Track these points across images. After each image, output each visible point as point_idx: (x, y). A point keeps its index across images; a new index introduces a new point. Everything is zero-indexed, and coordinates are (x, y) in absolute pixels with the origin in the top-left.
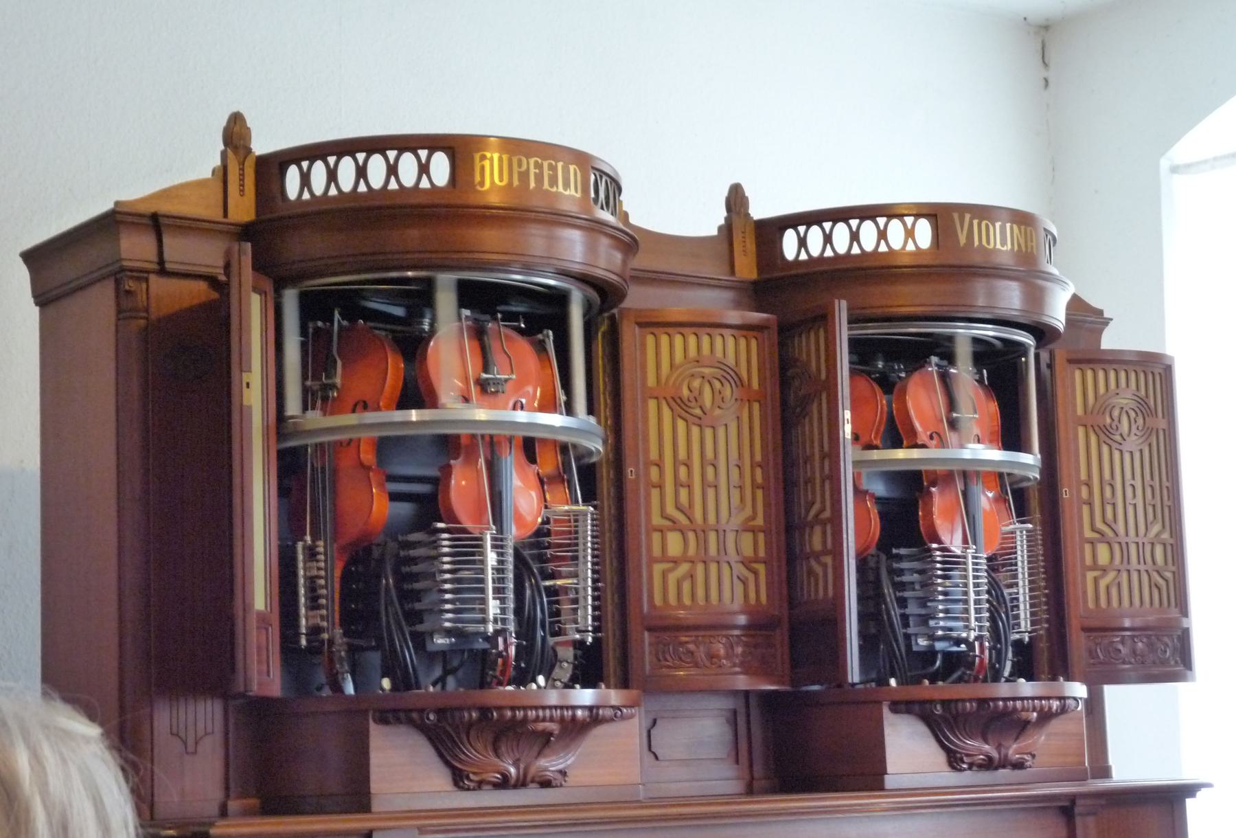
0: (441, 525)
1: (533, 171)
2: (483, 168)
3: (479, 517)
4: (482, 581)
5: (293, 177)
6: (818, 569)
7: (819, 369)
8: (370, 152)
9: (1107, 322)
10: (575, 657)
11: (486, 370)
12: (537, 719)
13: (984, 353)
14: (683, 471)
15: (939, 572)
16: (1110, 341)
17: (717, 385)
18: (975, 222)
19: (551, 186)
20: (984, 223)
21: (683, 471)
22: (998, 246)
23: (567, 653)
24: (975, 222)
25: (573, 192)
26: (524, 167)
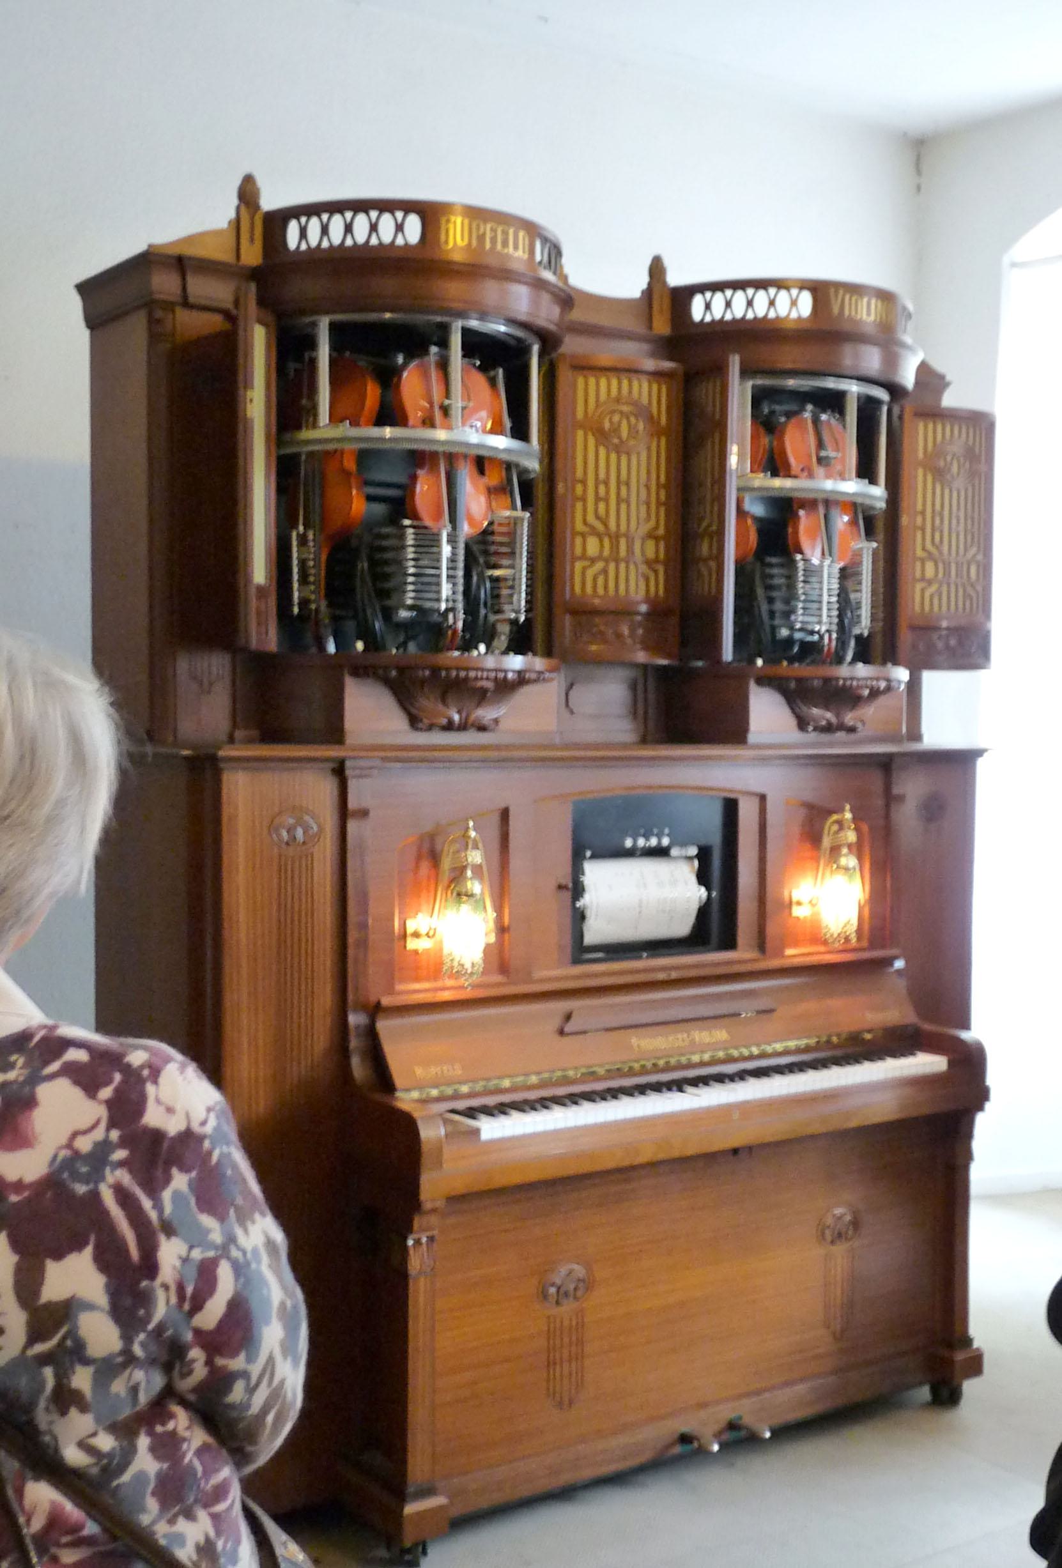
12: (476, 678)
16: (949, 400)
17: (633, 420)
18: (847, 297)
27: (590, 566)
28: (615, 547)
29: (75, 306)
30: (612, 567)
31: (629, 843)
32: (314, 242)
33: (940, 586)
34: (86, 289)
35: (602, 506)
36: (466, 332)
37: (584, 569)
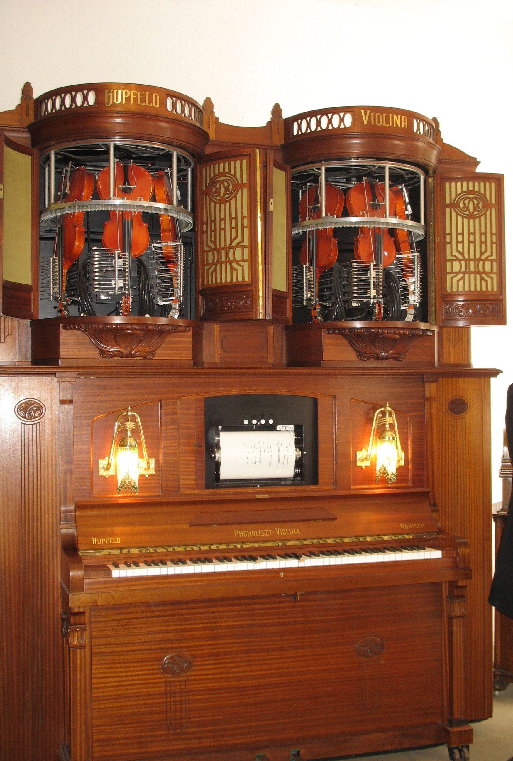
0: (353, 260)
1: (132, 96)
2: (109, 96)
3: (370, 257)
4: (369, 282)
5: (296, 126)
8: (333, 114)
9: (478, 163)
10: (414, 313)
11: (374, 200)
13: (397, 178)
14: (483, 239)
15: (355, 280)
16: (479, 169)
17: (476, 202)
18: (372, 114)
19: (142, 102)
21: (483, 239)
23: (411, 311)
24: (372, 114)
25: (154, 105)
27: (455, 276)
28: (468, 266)
30: (467, 276)
31: (246, 422)
32: (313, 129)
33: (217, 266)
35: (460, 246)
36: (116, 147)
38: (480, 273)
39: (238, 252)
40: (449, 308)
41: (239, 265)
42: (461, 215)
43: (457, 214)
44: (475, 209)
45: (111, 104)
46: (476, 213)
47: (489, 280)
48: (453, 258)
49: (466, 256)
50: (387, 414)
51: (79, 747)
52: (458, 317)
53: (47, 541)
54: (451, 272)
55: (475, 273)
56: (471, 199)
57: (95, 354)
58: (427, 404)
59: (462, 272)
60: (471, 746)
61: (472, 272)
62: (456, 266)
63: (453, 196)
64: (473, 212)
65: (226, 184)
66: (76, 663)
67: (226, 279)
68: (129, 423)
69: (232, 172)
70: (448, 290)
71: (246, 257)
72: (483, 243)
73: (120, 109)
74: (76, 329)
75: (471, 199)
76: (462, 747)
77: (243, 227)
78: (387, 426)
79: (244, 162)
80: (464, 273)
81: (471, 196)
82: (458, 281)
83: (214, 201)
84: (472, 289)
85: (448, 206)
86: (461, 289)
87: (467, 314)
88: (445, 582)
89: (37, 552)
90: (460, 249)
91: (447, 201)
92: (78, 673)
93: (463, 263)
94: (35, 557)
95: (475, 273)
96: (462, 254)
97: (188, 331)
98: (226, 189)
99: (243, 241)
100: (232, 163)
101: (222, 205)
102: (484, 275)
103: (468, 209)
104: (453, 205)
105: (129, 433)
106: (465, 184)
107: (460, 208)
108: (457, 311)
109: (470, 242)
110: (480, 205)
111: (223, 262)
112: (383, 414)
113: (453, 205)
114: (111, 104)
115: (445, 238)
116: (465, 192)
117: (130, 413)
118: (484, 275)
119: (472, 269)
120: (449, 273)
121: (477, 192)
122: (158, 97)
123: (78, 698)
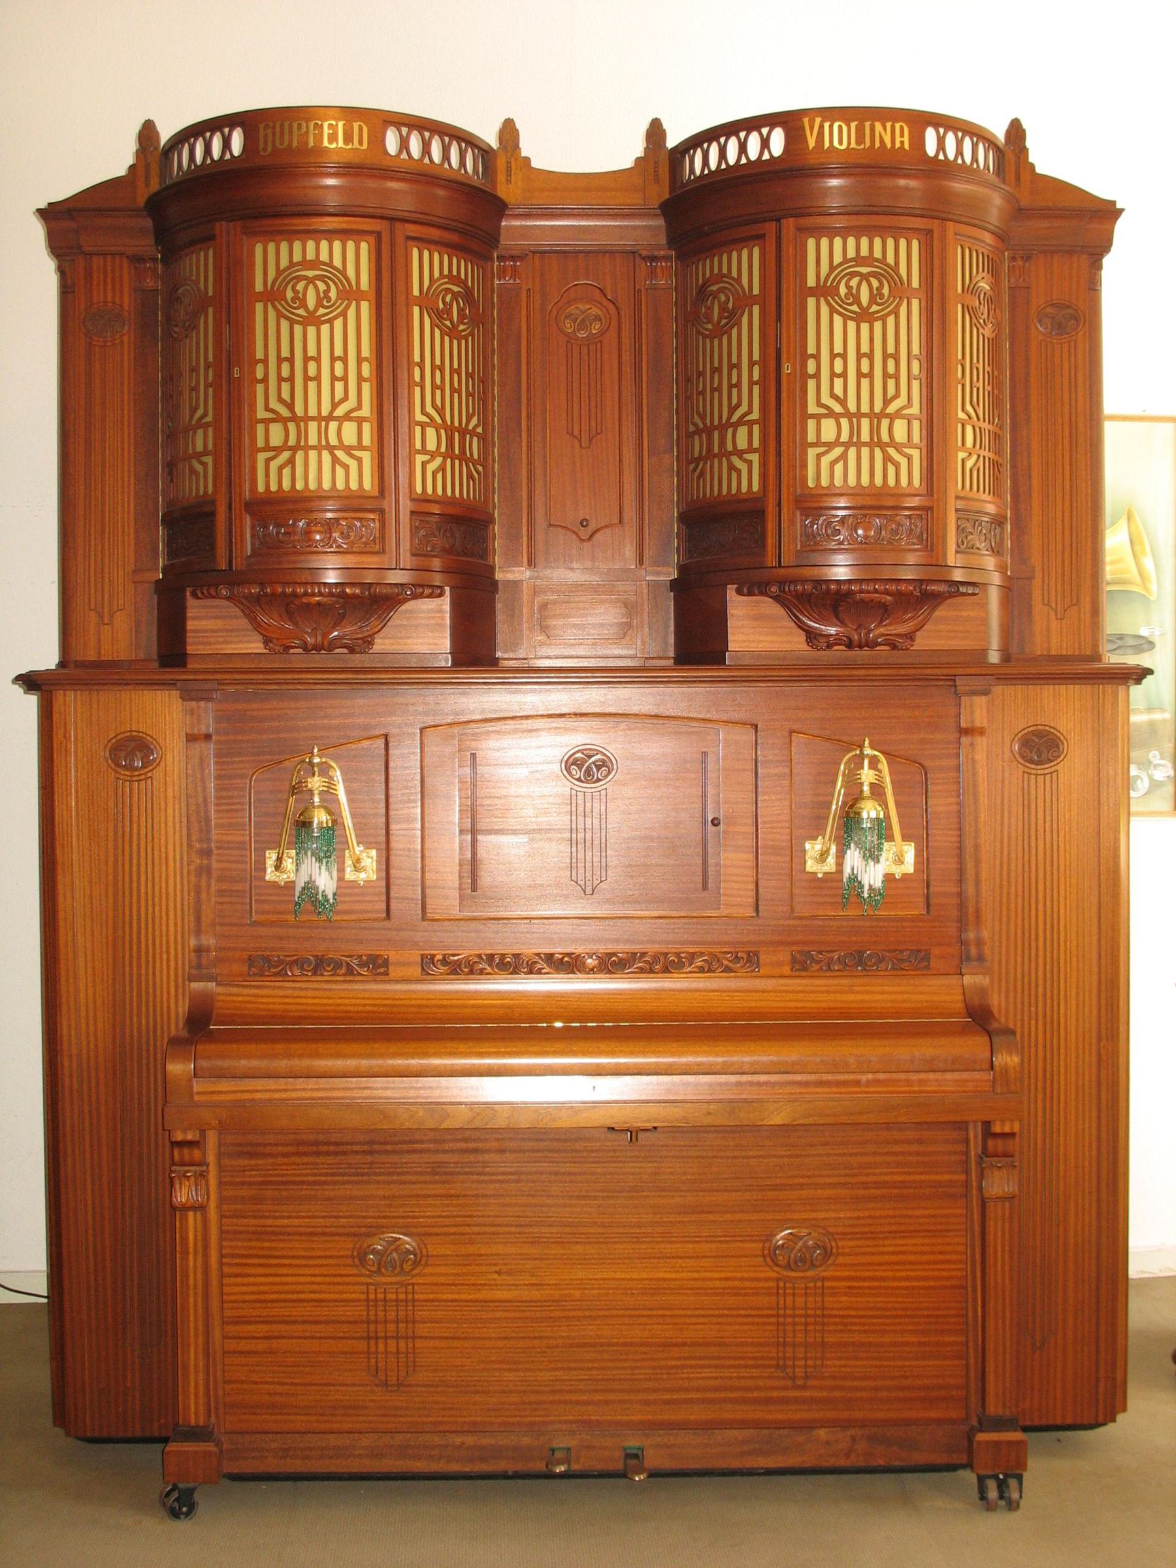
6: (199, 468)
7: (206, 287)
8: (772, 127)
12: (306, 594)
18: (827, 125)
19: (330, 142)
20: (836, 125)
22: (326, 143)
26: (304, 129)
28: (855, 430)
29: (37, 232)
30: (852, 452)
34: (51, 214)
35: (838, 382)
37: (268, 461)
38: (883, 446)
39: (742, 432)
40: (812, 523)
41: (352, 456)
42: (840, 314)
43: (832, 311)
44: (872, 300)
45: (269, 149)
46: (874, 308)
47: (903, 462)
48: (824, 411)
49: (852, 407)
50: (866, 762)
51: (192, 1397)
52: (833, 545)
53: (165, 1005)
54: (818, 444)
55: (871, 445)
56: (865, 277)
57: (796, 642)
58: (965, 740)
59: (843, 444)
60: (1026, 1476)
61: (865, 444)
62: (828, 430)
63: (825, 269)
64: (869, 306)
65: (723, 298)
66: (187, 1237)
67: (720, 490)
68: (316, 778)
69: (734, 274)
70: (811, 484)
71: (367, 441)
72: (865, 376)
73: (335, 158)
74: (213, 597)
75: (865, 277)
76: (1006, 1476)
77: (360, 379)
78: (866, 788)
79: (756, 251)
80: (847, 445)
81: (864, 270)
82: (833, 464)
83: (702, 334)
84: (865, 481)
85: (812, 292)
86: (838, 482)
87: (852, 540)
88: (975, 1122)
89: (148, 1023)
90: (838, 390)
91: (811, 282)
92: (191, 1258)
93: (844, 422)
94: (144, 1034)
95: (871, 445)
96: (843, 402)
97: (441, 595)
98: (723, 309)
99: (359, 406)
100: (745, 253)
101: (716, 342)
102: (891, 451)
103: (857, 301)
104: (824, 291)
105: (316, 799)
106: (851, 241)
107: (840, 298)
108: (829, 531)
109: (860, 375)
110: (886, 291)
111: (715, 456)
112: (858, 761)
113: (824, 291)
114: (269, 149)
115: (804, 365)
116: (851, 260)
117: (316, 760)
118: (891, 451)
119: (865, 437)
120: (813, 445)
121: (877, 260)
122: (365, 129)
123: (192, 1304)
